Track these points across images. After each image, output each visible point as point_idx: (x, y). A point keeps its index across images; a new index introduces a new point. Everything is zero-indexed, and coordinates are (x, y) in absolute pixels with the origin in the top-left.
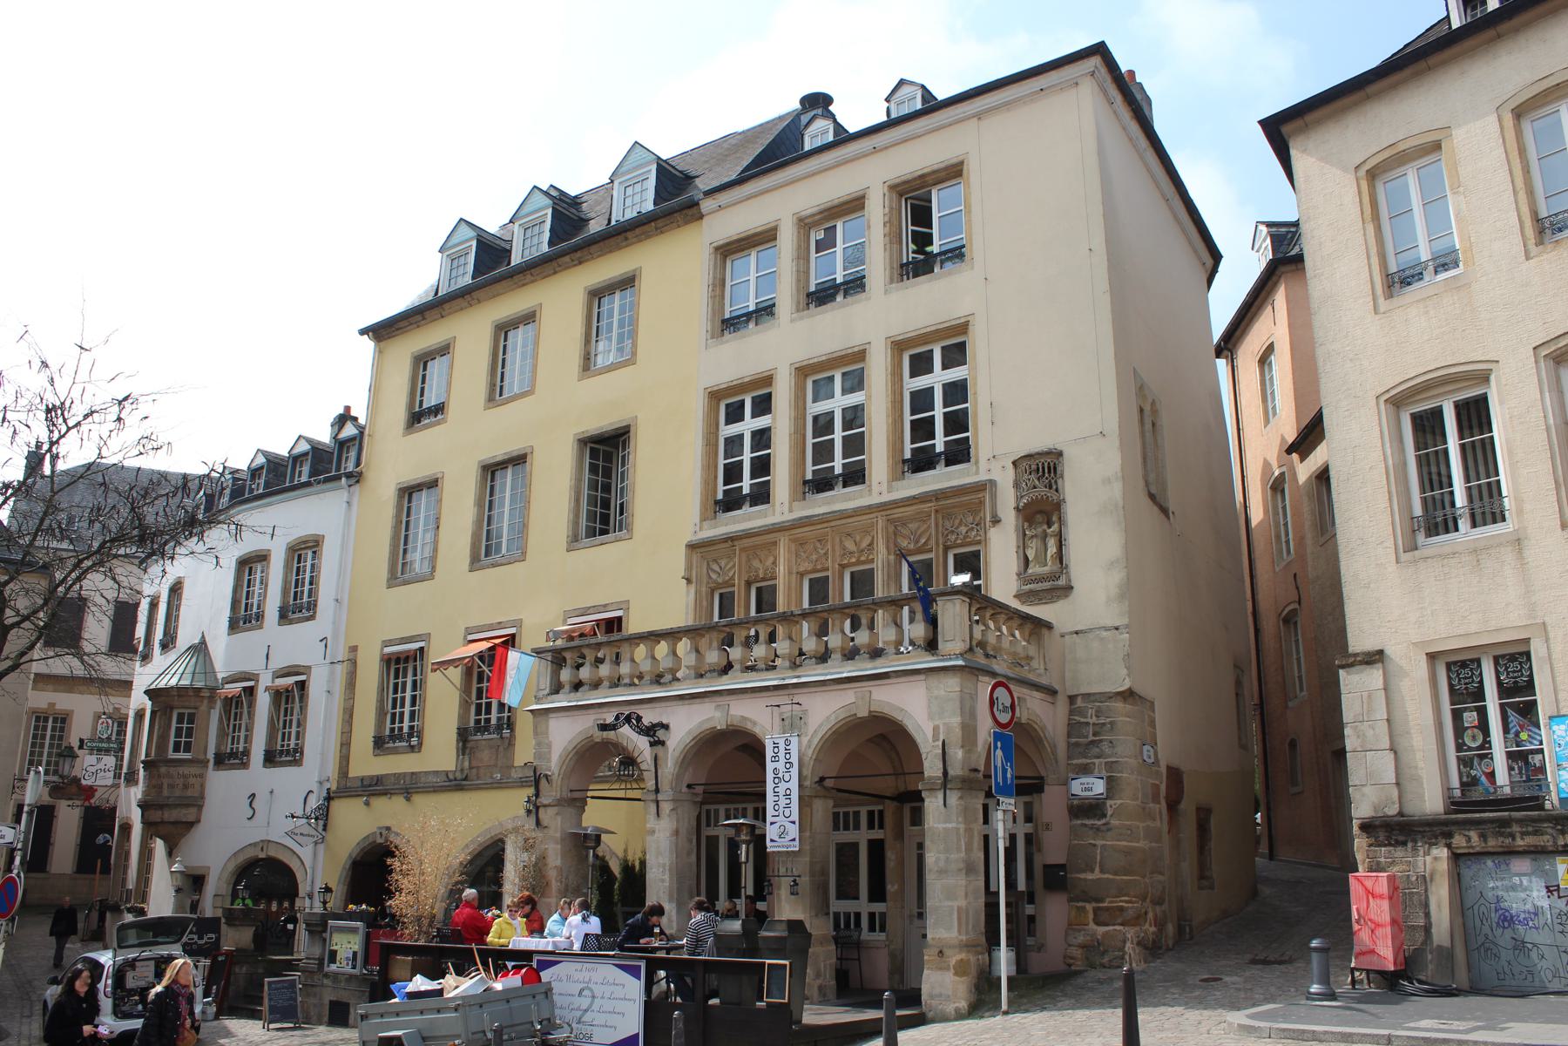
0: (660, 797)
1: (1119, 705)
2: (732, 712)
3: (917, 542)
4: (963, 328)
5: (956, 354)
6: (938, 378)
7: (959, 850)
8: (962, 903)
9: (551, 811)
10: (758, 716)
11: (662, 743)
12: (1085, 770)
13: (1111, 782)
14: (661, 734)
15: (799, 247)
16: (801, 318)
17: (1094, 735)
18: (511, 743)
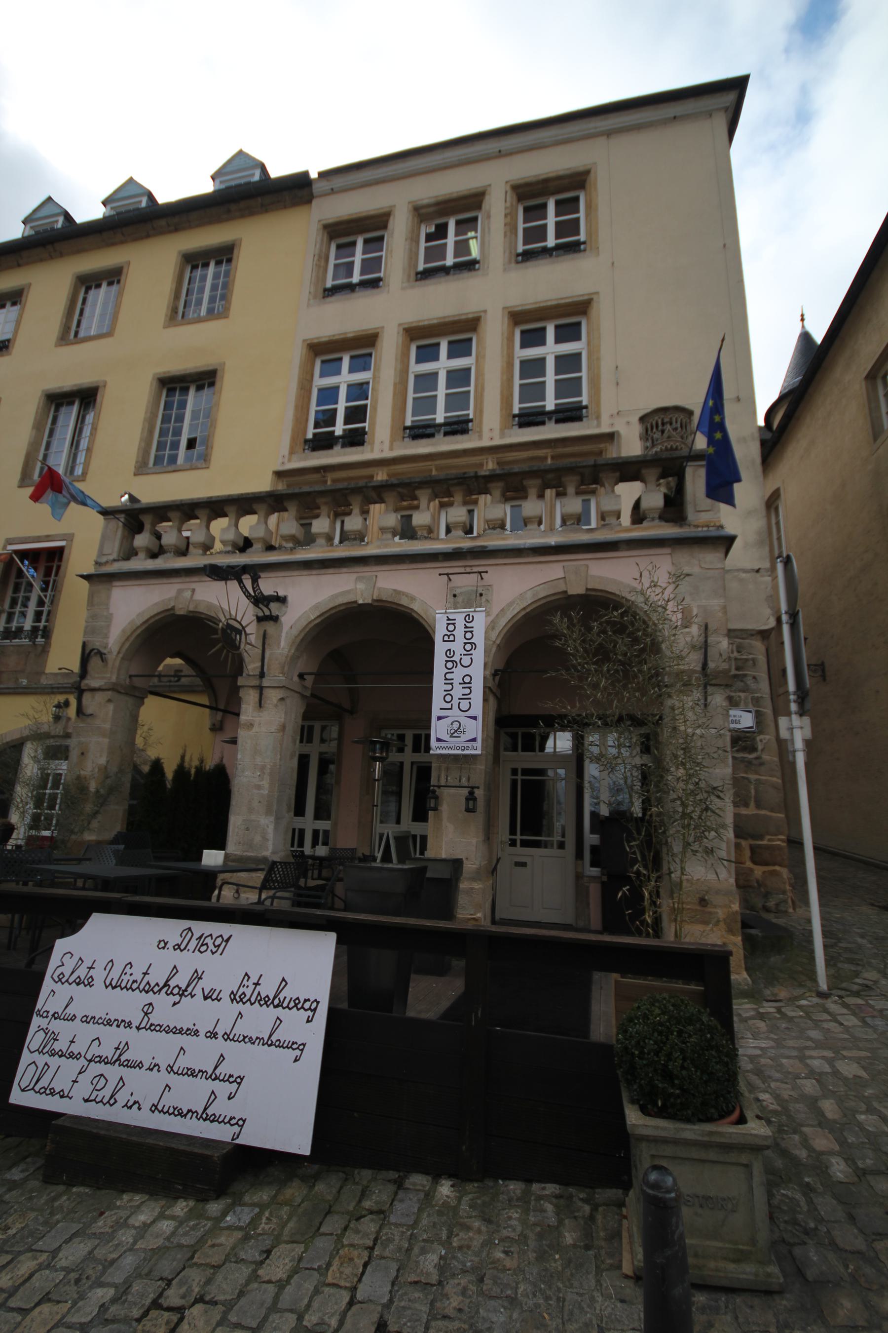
0: (266, 682)
9: (100, 697)
10: (419, 590)
11: (275, 619)
14: (274, 607)
16: (375, 329)
17: (737, 669)
18: (45, 650)
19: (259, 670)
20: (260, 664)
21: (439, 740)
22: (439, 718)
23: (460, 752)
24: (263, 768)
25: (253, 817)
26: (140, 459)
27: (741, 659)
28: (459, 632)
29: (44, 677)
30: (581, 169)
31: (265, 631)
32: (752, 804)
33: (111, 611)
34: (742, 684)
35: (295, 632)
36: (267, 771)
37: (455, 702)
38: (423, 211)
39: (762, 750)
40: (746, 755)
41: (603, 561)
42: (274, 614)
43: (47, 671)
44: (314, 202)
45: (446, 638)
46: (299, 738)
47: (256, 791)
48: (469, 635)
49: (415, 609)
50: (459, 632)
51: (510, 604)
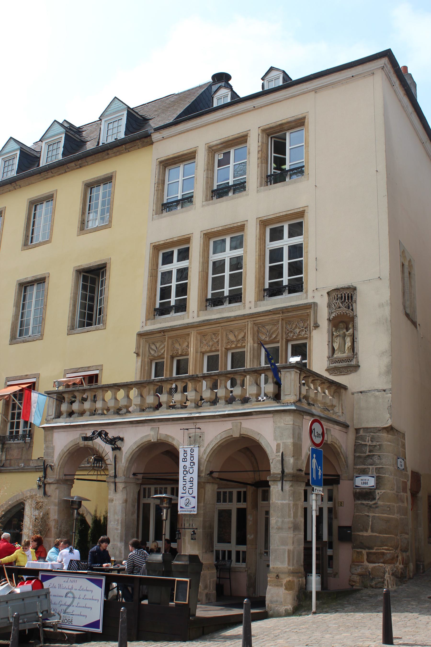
1: (384, 435)
2: (243, 426)
3: (271, 337)
4: (301, 214)
5: (297, 230)
6: (286, 242)
7: (289, 517)
8: (291, 547)
9: (53, 487)
10: (175, 435)
11: (119, 449)
12: (364, 472)
13: (379, 480)
14: (119, 443)
15: (208, 163)
18: (30, 446)
19: (114, 474)
20: (114, 471)
21: (181, 507)
22: (182, 498)
23: (189, 513)
24: (118, 520)
25: (115, 543)
26: (70, 324)
27: (372, 446)
28: (188, 457)
29: (31, 462)
30: (300, 116)
31: (115, 455)
32: (369, 530)
33: (54, 445)
34: (371, 460)
35: (128, 455)
36: (120, 522)
37: (187, 490)
38: (213, 148)
39: (378, 499)
40: (370, 502)
41: (247, 420)
42: (119, 446)
43: (33, 458)
44: (154, 145)
45: (184, 460)
46: (137, 504)
47: (116, 531)
48: (192, 459)
49: (175, 444)
50: (188, 457)
51: (212, 441)
